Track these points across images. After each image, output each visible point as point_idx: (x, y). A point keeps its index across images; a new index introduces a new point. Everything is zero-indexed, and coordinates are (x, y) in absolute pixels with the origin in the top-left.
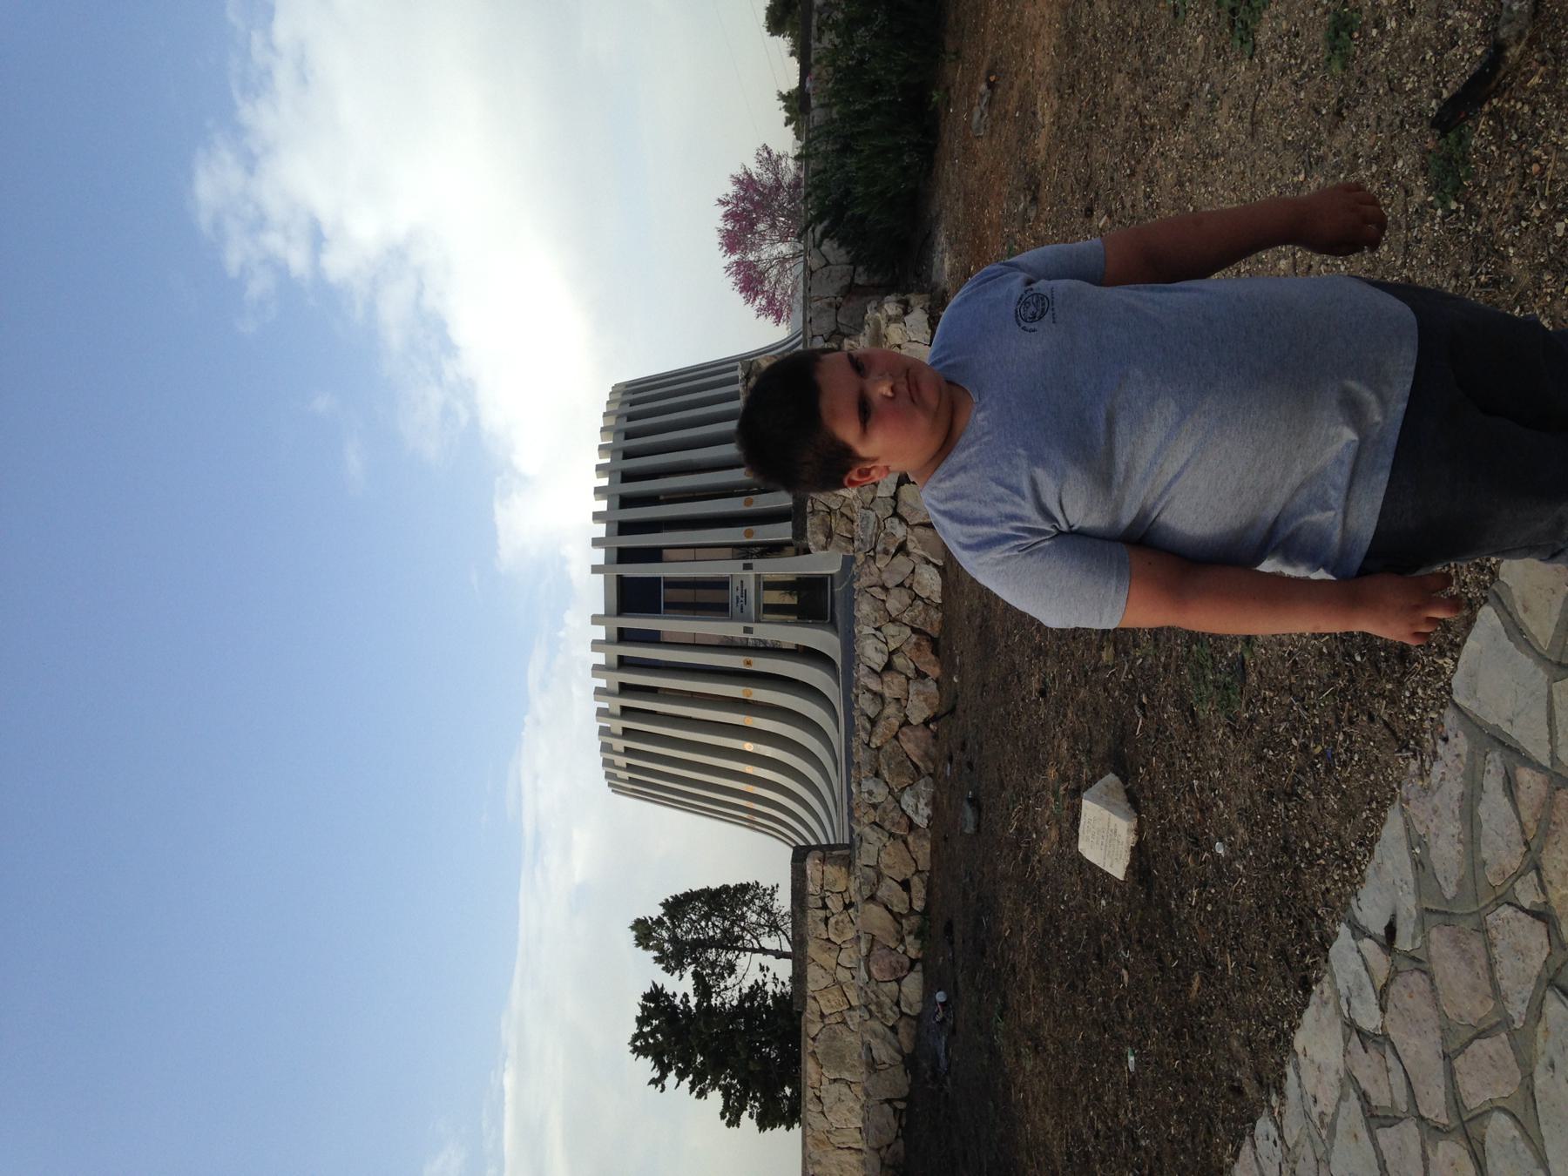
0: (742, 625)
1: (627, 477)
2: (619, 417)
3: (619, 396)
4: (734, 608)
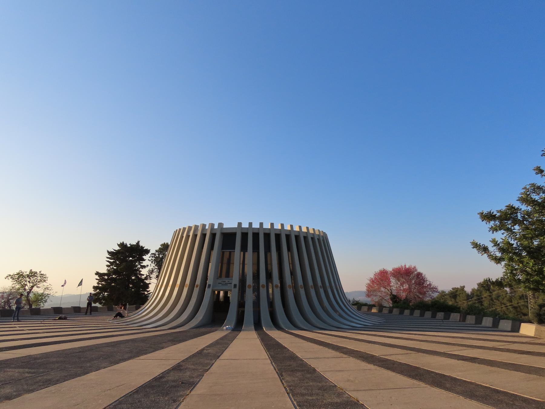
0: (212, 284)
1: (288, 237)
2: (319, 235)
3: (322, 234)
4: (220, 281)
